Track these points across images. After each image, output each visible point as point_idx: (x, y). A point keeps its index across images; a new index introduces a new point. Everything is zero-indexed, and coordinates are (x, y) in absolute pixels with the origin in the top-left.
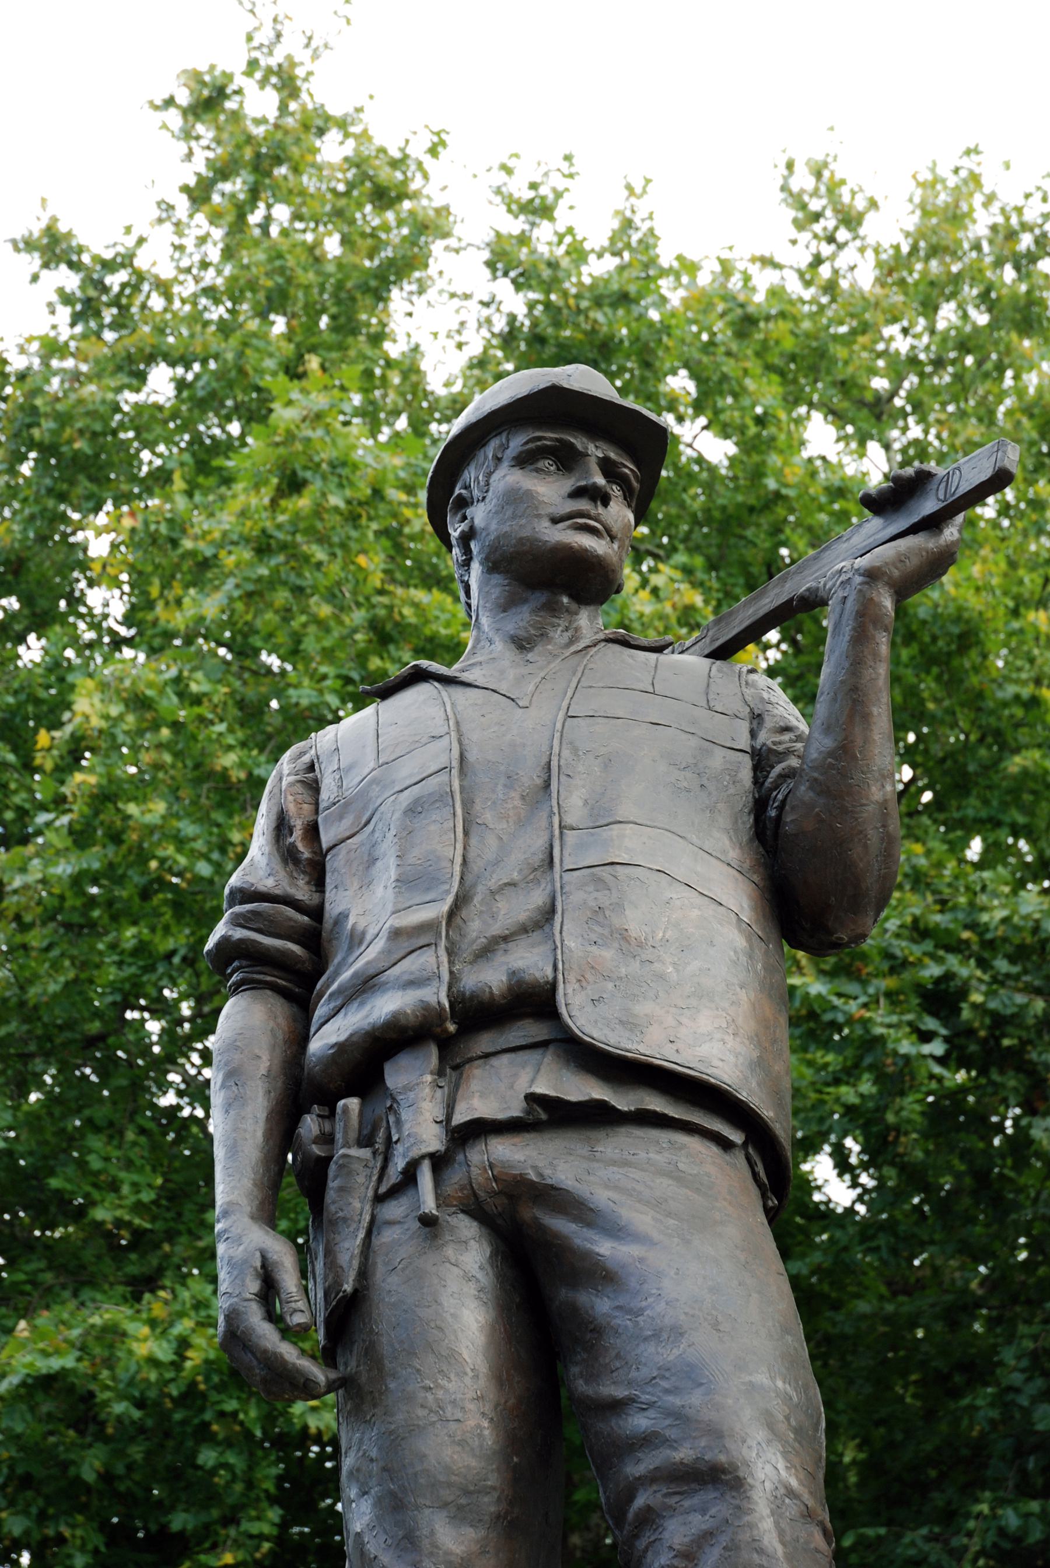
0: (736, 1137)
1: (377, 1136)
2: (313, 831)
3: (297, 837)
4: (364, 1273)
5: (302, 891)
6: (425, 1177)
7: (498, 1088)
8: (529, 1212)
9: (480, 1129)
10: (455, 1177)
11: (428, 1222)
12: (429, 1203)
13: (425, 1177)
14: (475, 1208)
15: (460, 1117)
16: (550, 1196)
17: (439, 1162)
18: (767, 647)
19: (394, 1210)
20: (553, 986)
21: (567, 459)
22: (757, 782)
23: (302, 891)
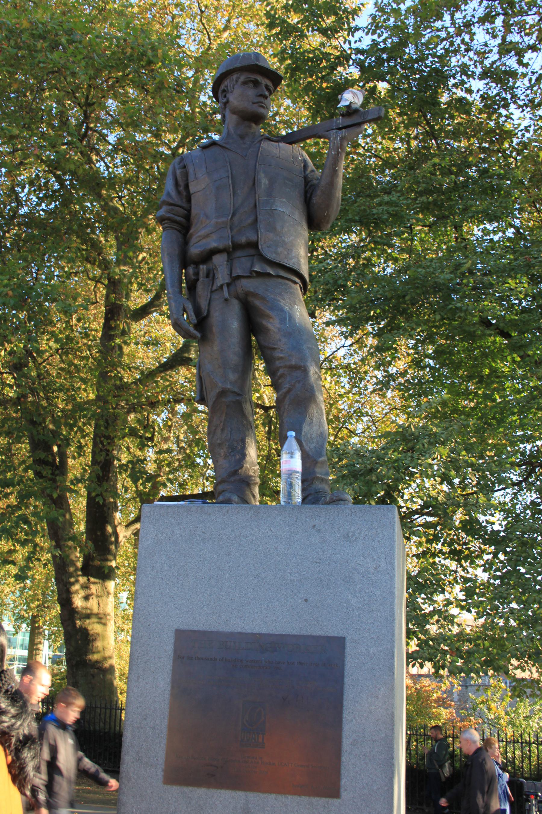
0: (298, 280)
1: (211, 275)
2: (187, 186)
3: (181, 188)
4: (209, 311)
5: (185, 205)
6: (225, 289)
7: (242, 266)
8: (250, 299)
9: (239, 277)
10: (232, 288)
11: (226, 300)
12: (226, 295)
13: (225, 289)
14: (238, 298)
15: (234, 274)
16: (255, 295)
17: (228, 285)
18: (499, 433)
19: (215, 296)
20: (257, 243)
21: (256, 84)
22: (305, 186)
23: (185, 205)
